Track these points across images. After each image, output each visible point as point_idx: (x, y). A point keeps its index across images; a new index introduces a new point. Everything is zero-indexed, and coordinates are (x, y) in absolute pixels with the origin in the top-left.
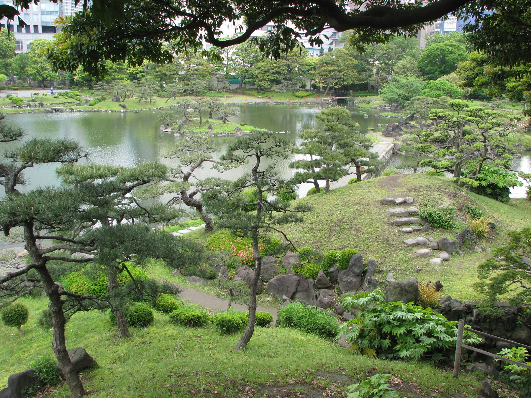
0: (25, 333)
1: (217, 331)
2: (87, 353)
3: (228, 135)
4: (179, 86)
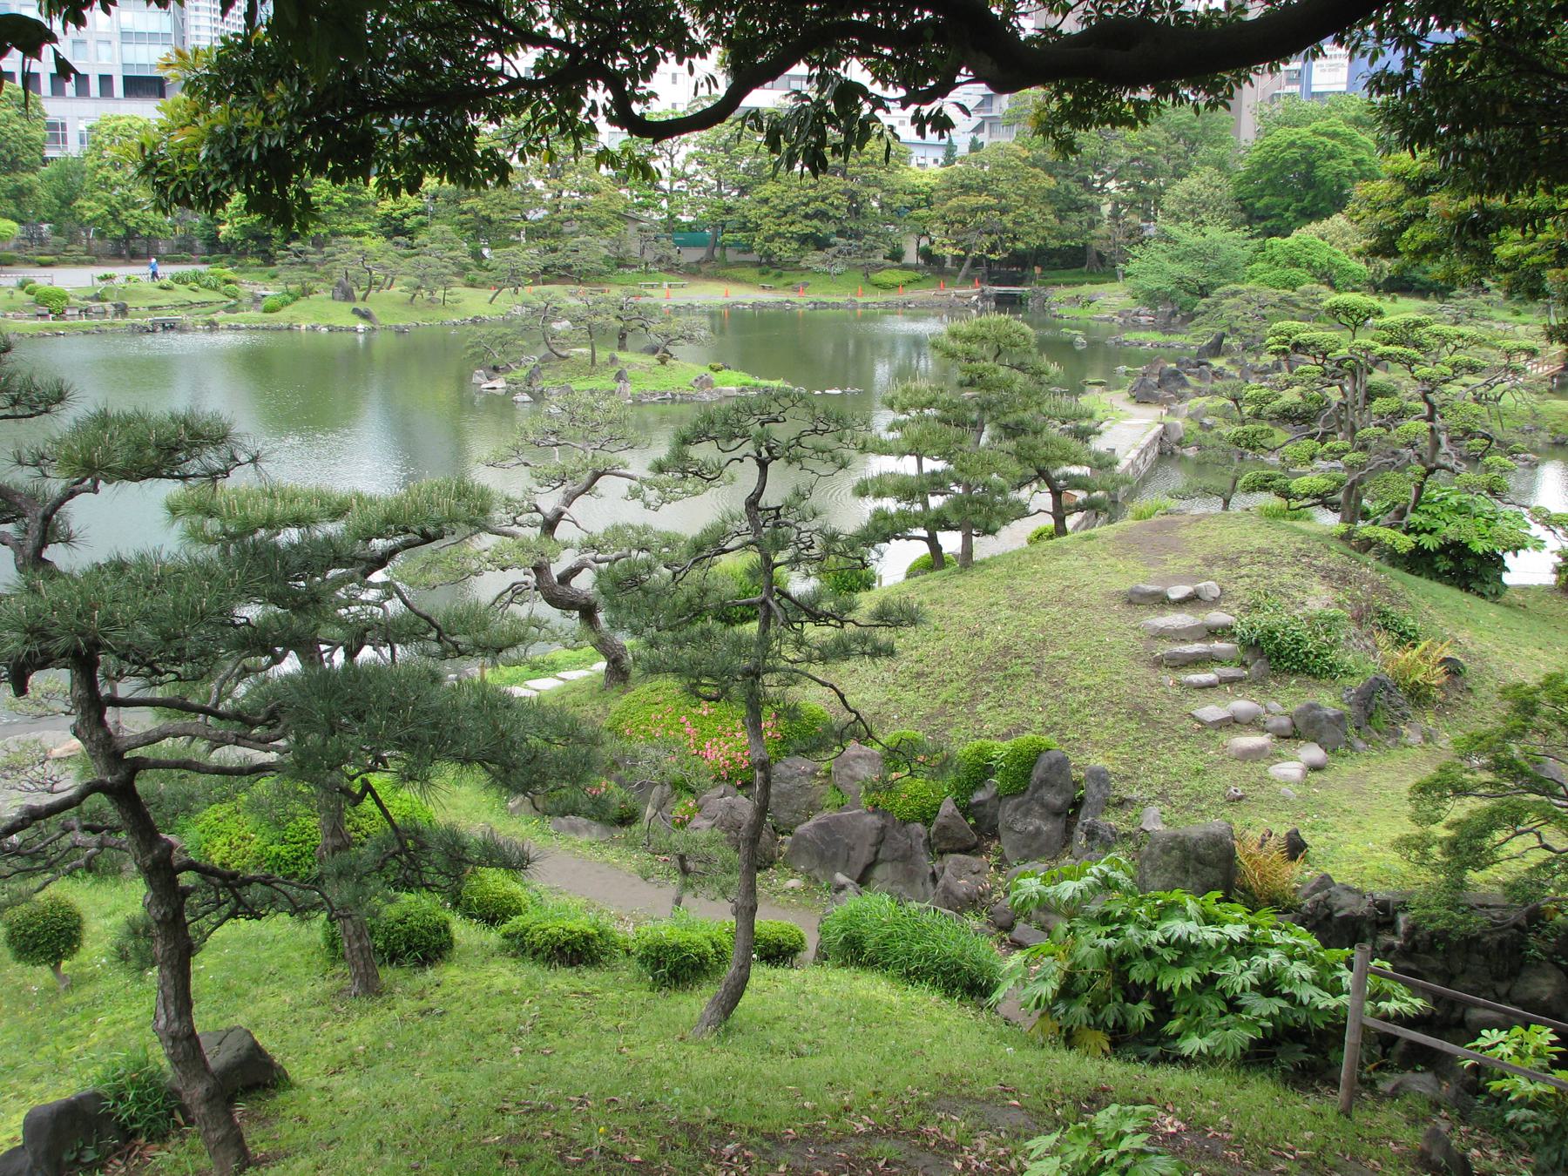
0: (72, 984)
1: (640, 979)
2: (255, 1043)
3: (673, 400)
4: (528, 254)
